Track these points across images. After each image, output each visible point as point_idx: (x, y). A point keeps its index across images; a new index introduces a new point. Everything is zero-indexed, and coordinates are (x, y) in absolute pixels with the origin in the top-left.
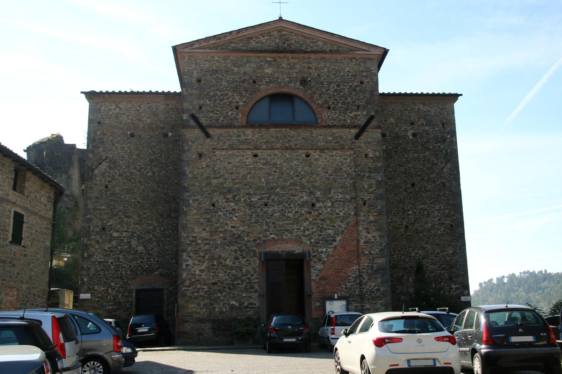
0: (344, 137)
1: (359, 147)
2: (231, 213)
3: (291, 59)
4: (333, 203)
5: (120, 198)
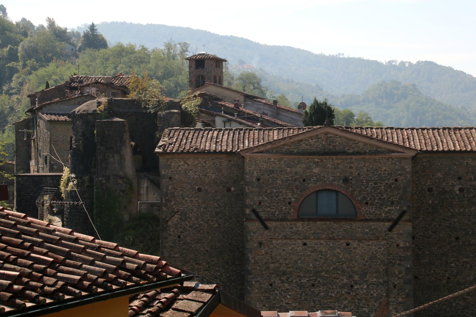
0: (379, 229)
1: (392, 238)
2: (285, 292)
4: (368, 285)
5: (191, 247)
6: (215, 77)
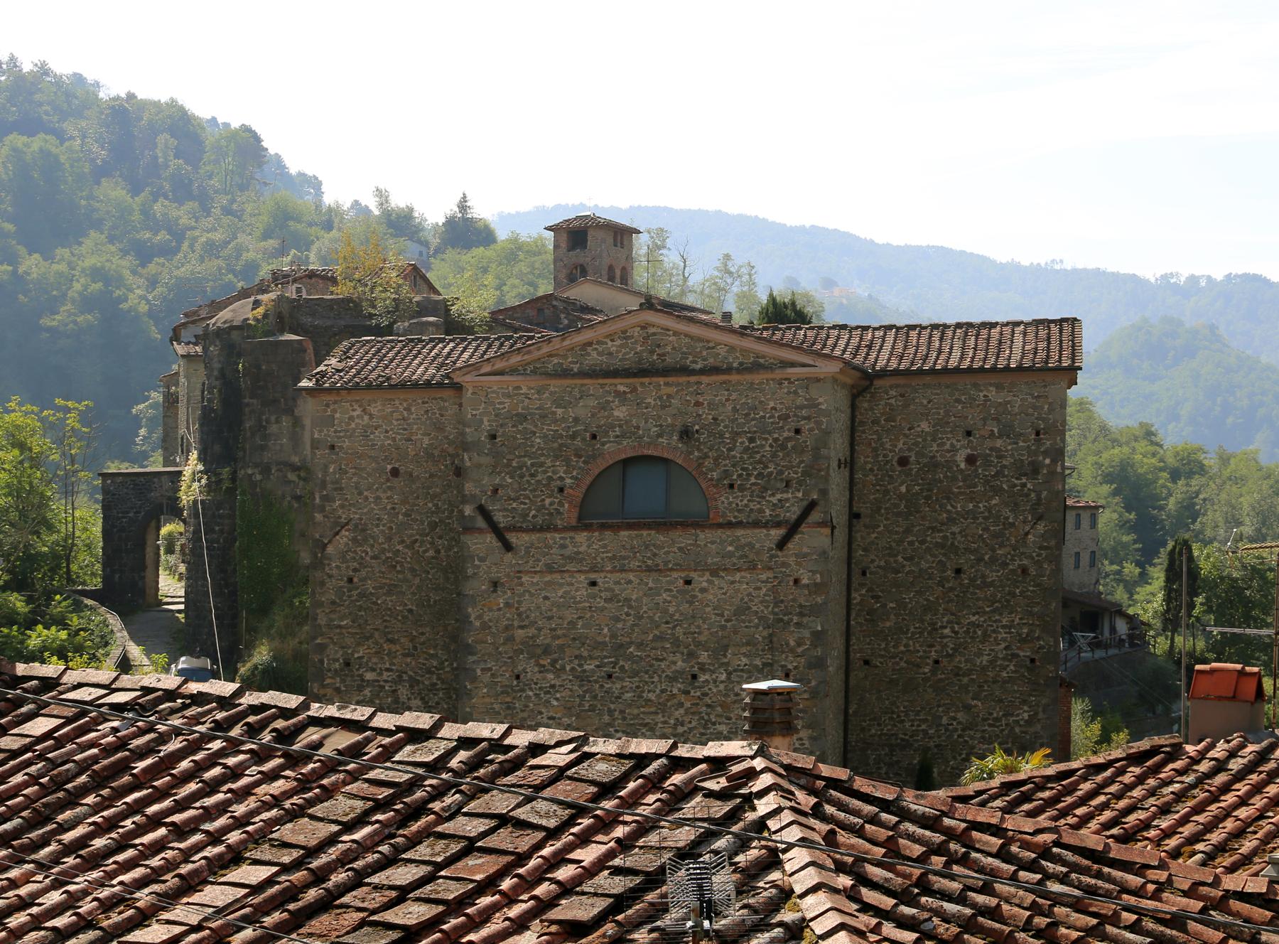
0: (757, 546)
1: (784, 564)
2: (548, 692)
4: (729, 674)
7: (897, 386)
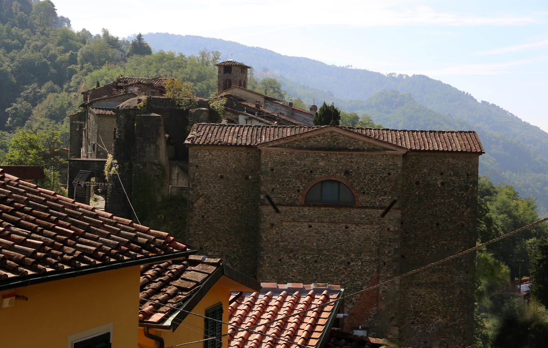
1: (384, 223)
3: (339, 155)
4: (362, 263)
5: (213, 226)
6: (240, 81)
7: (415, 155)
